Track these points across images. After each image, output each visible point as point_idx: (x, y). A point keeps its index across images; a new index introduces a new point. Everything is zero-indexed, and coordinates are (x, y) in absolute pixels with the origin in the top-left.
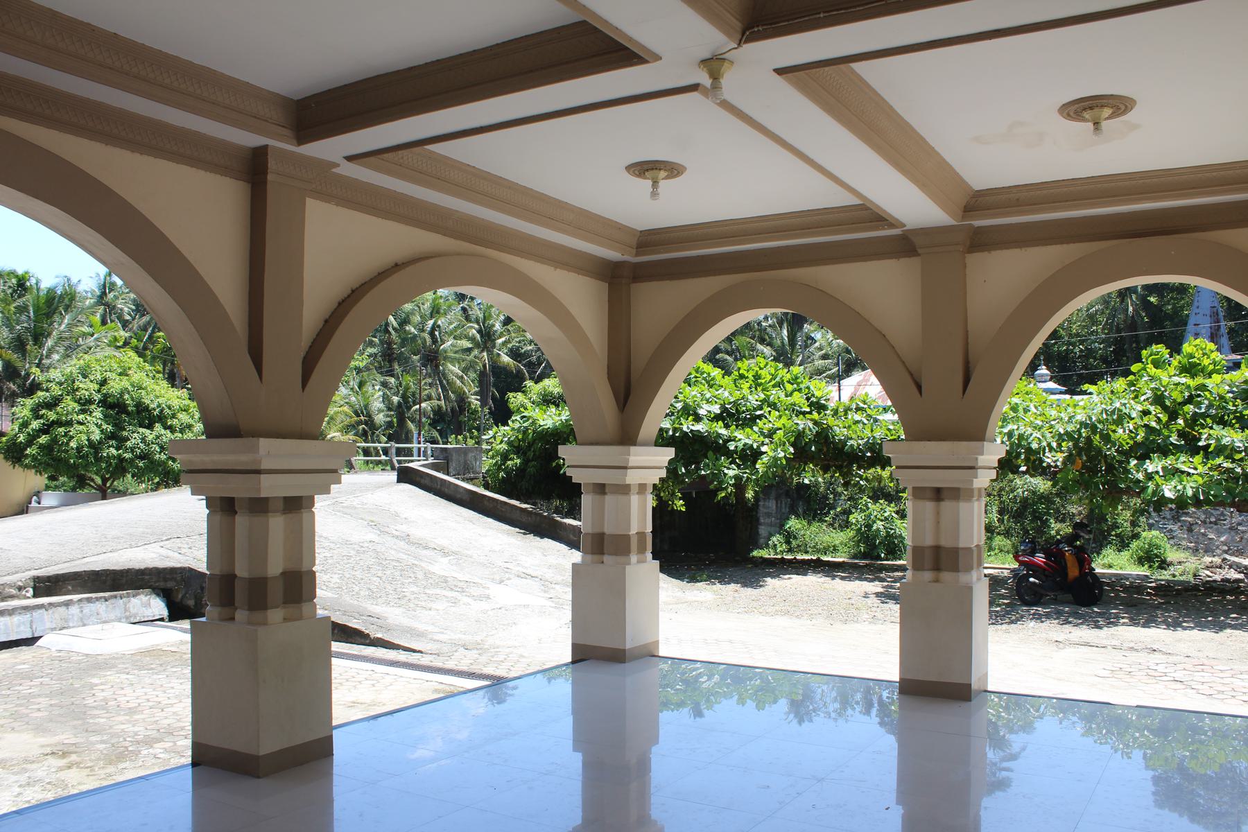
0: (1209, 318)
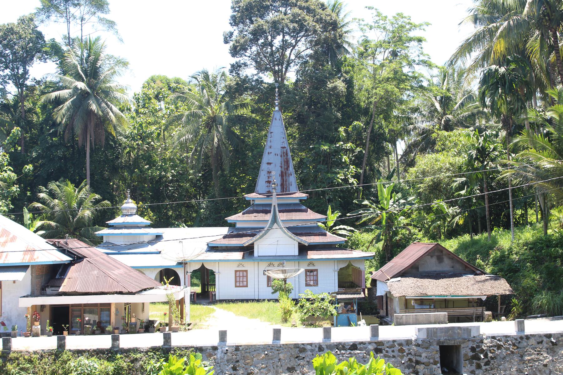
0: (280, 157)
